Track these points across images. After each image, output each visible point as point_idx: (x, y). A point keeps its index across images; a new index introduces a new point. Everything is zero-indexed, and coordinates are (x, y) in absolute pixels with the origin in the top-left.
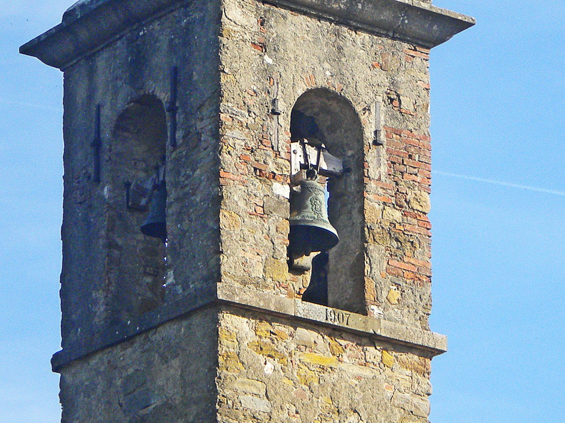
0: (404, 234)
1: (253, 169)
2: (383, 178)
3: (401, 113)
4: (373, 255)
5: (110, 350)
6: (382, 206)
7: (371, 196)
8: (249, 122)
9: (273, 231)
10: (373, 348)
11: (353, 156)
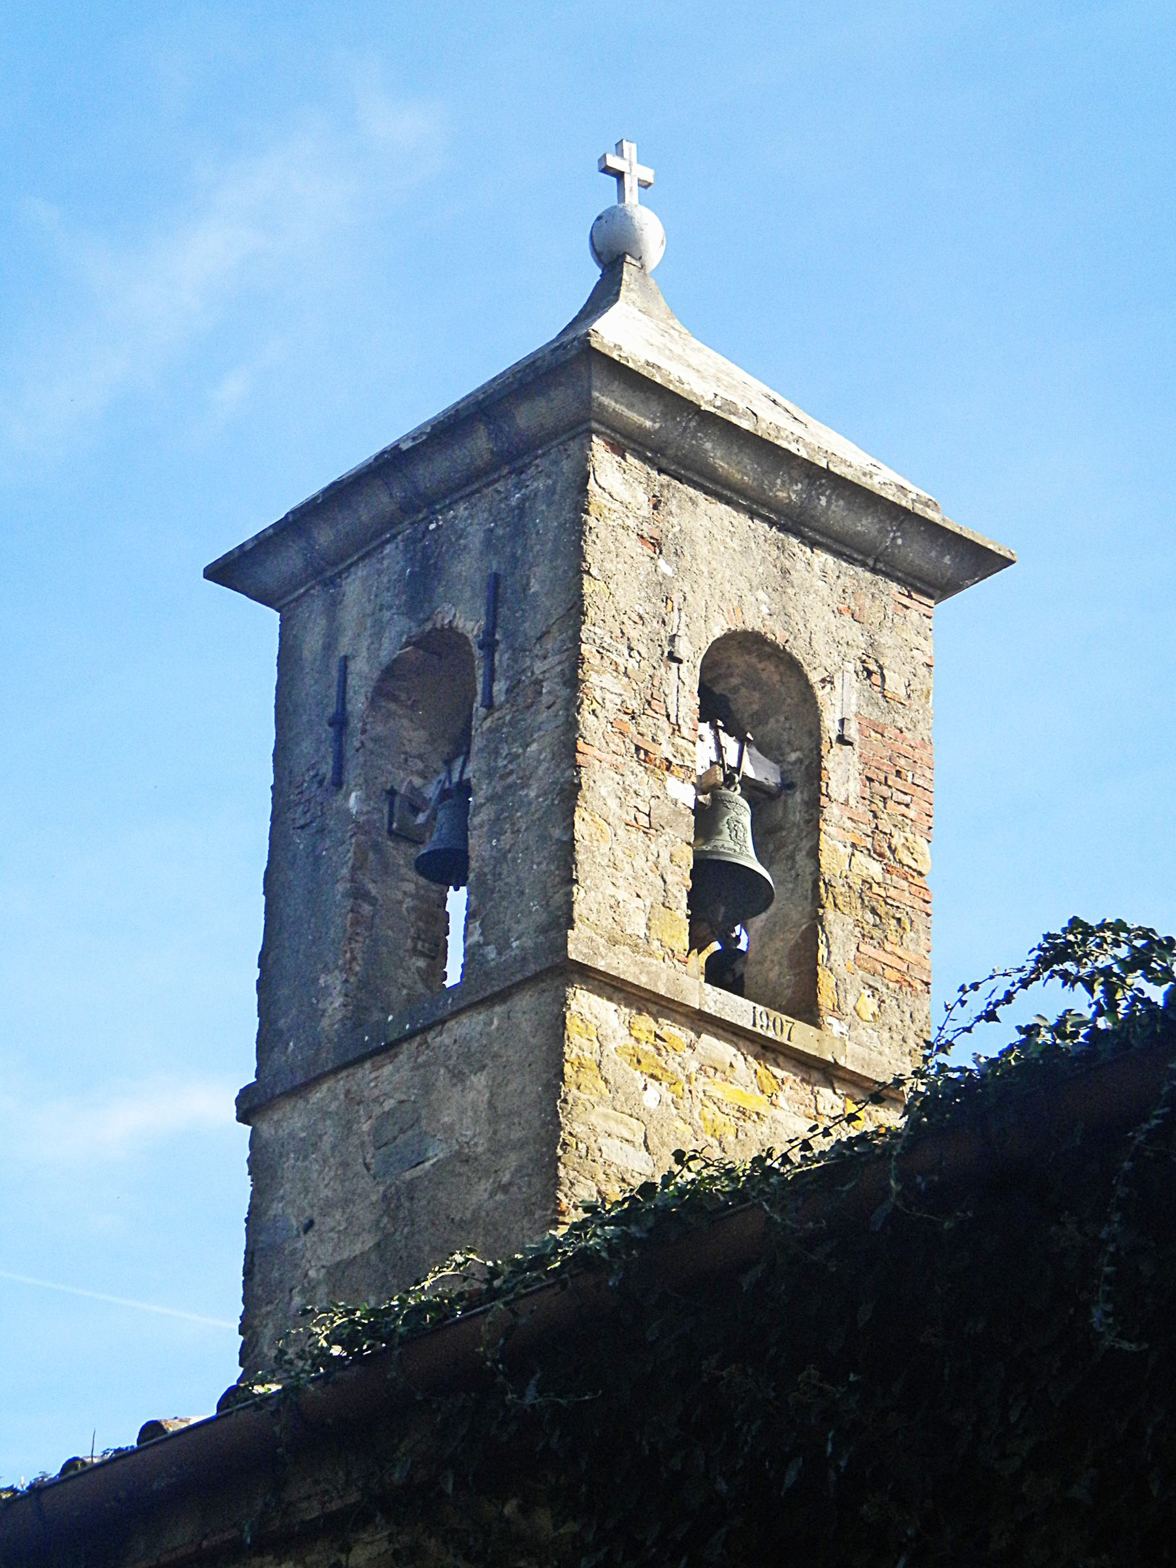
0: (886, 903)
1: (633, 747)
2: (852, 802)
3: (885, 697)
4: (834, 931)
5: (351, 1071)
6: (849, 850)
7: (831, 830)
8: (630, 667)
9: (664, 860)
10: (831, 1091)
11: (800, 761)
